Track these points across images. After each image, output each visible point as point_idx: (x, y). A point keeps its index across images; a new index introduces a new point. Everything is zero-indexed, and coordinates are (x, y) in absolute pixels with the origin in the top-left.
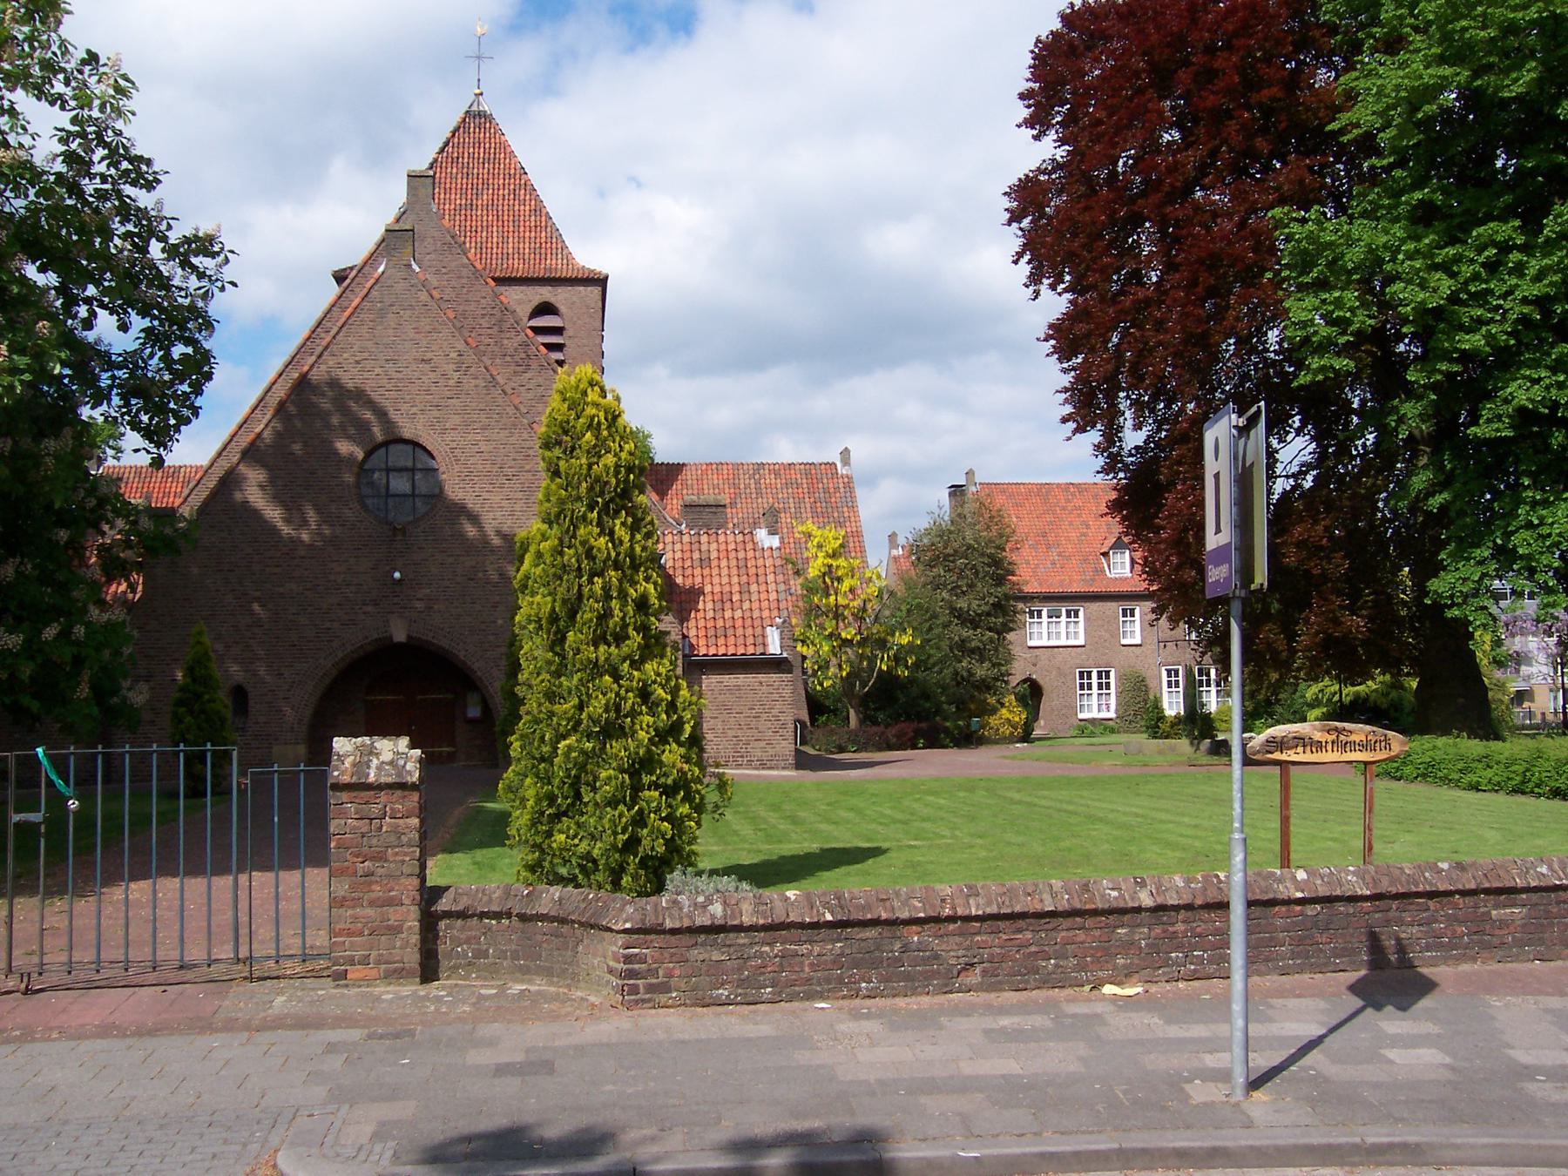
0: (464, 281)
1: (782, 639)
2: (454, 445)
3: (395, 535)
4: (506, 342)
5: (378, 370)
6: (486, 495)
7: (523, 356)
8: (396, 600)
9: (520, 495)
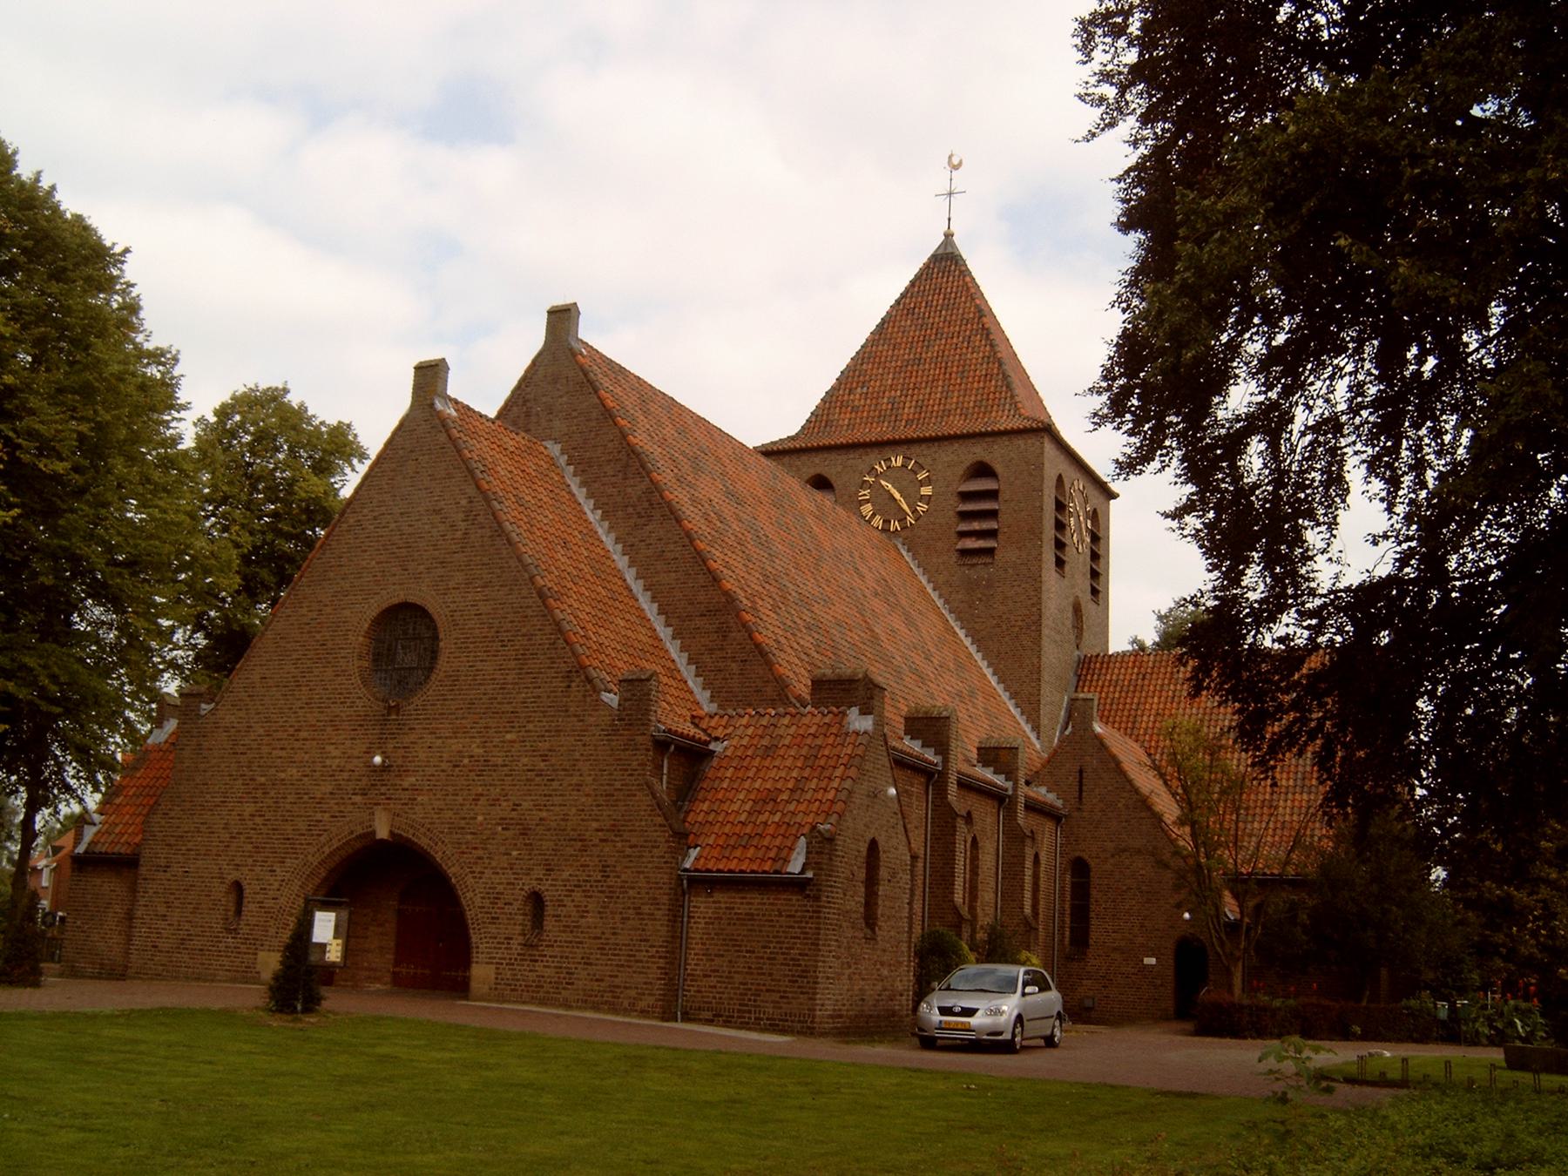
0: (594, 424)
3: (389, 714)
4: (629, 490)
7: (646, 505)
8: (383, 789)
9: (512, 664)
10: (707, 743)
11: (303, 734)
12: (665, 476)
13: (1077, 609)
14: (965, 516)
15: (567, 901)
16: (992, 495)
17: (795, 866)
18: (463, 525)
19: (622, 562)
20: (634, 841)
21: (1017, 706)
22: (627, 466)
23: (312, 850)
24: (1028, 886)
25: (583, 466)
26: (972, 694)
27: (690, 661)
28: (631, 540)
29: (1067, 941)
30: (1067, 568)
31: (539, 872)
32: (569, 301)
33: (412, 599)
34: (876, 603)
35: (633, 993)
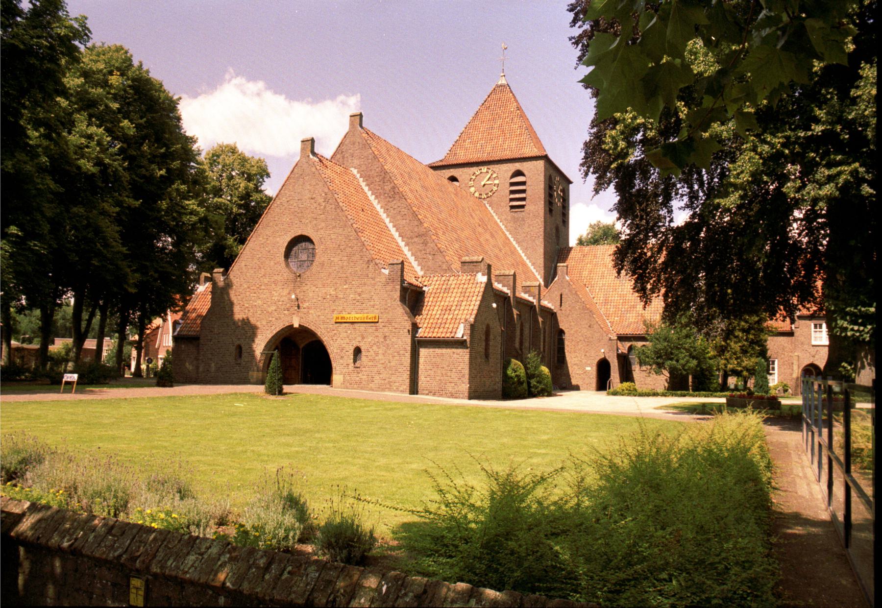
1: (465, 329)
2: (321, 236)
5: (295, 204)
6: (332, 259)
9: (345, 258)
10: (422, 287)
11: (263, 287)
12: (399, 182)
13: (557, 229)
14: (512, 192)
15: (370, 350)
16: (524, 183)
17: (459, 335)
18: (323, 204)
19: (384, 216)
20: (396, 326)
21: (534, 268)
22: (384, 178)
23: (268, 332)
24: (542, 341)
25: (367, 178)
26: (518, 265)
27: (412, 255)
28: (387, 207)
29: (556, 361)
30: (553, 212)
31: (359, 339)
32: (571, 179)
33: (304, 233)
34: (480, 230)
35: (397, 384)
